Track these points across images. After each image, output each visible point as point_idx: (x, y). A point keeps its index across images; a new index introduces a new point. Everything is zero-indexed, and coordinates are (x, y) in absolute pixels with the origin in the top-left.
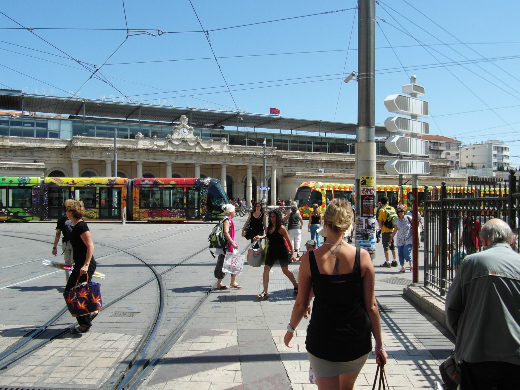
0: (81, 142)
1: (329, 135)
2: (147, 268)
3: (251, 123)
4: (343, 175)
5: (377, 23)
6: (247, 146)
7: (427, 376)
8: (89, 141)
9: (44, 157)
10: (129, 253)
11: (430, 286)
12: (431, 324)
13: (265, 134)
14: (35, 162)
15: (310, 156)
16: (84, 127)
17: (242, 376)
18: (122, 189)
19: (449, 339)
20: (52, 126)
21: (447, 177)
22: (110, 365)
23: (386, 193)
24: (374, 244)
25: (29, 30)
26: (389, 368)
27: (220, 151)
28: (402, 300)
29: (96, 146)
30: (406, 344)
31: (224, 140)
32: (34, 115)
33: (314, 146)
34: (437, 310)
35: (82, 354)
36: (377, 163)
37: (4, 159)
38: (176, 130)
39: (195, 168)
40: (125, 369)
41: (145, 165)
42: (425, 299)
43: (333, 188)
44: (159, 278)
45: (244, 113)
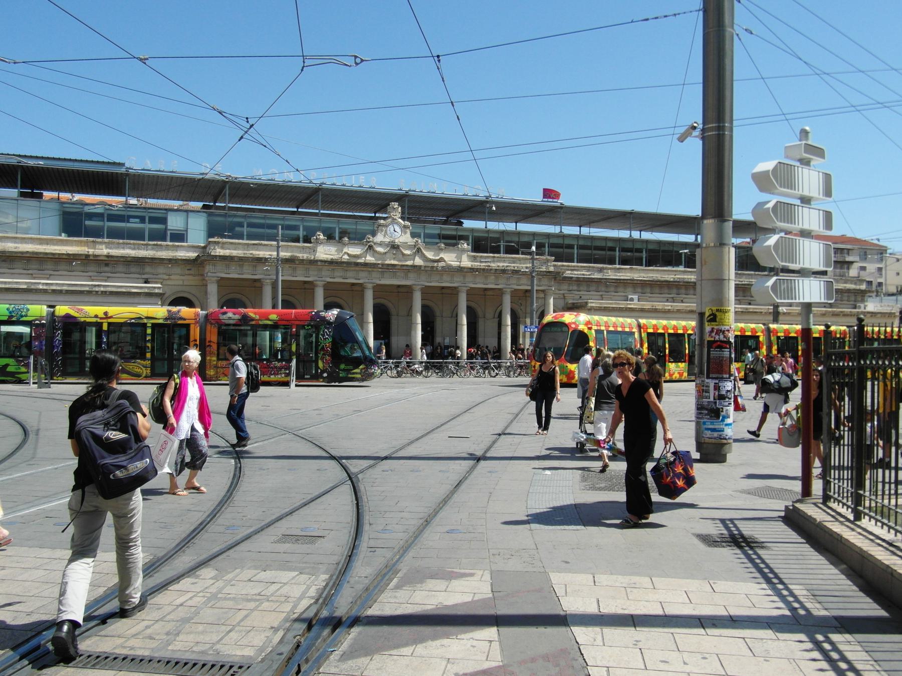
0: (222, 248)
1: (647, 235)
2: (333, 463)
3: (510, 215)
4: (672, 306)
5: (738, 35)
6: (502, 255)
7: (833, 663)
8: (235, 246)
9: (160, 274)
10: (304, 437)
11: (834, 502)
12: (836, 571)
13: (534, 235)
14: (146, 282)
15: (613, 273)
16: (227, 224)
17: (502, 650)
18: (192, 326)
19: (871, 598)
20: (175, 223)
21: (860, 310)
22: (276, 625)
23: (686, 336)
24: (730, 427)
25: (141, 60)
26: (763, 646)
27: (455, 264)
28: (782, 527)
29: (246, 256)
30: (792, 605)
31: (463, 244)
32: (144, 204)
33: (619, 255)
34: (848, 546)
35: (230, 604)
36: (735, 284)
37: (95, 278)
38: (380, 228)
39: (412, 293)
40: (302, 631)
41: (328, 287)
42: (825, 526)
43: (653, 329)
44: (353, 479)
45: (497, 198)
